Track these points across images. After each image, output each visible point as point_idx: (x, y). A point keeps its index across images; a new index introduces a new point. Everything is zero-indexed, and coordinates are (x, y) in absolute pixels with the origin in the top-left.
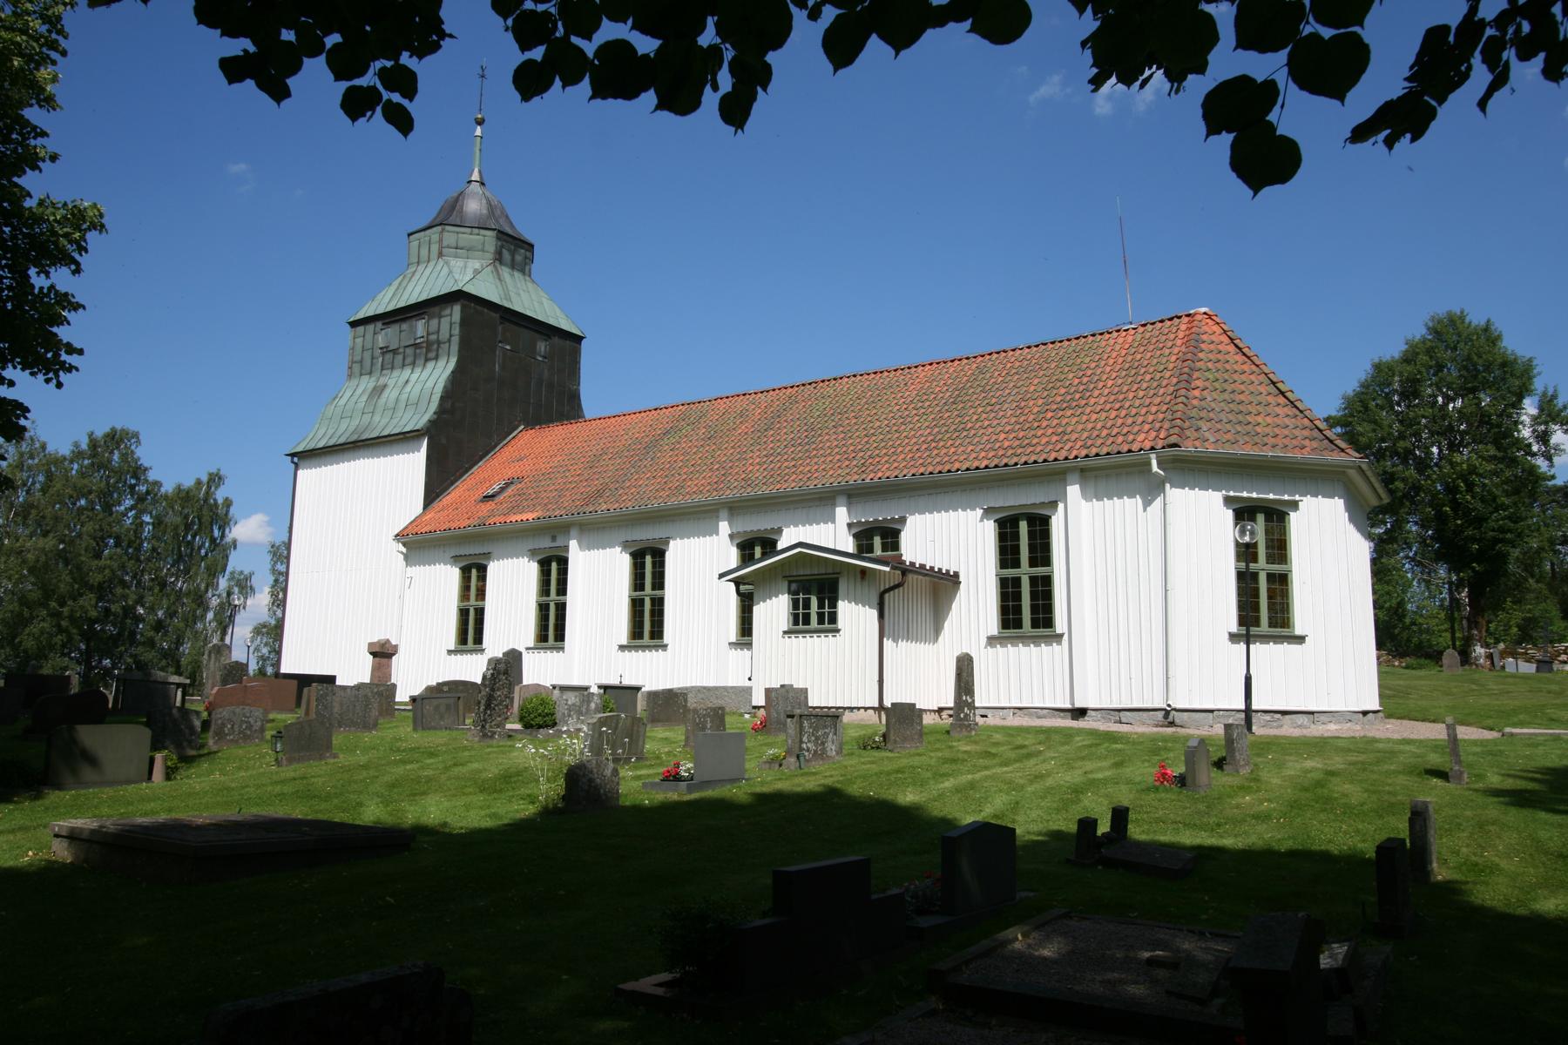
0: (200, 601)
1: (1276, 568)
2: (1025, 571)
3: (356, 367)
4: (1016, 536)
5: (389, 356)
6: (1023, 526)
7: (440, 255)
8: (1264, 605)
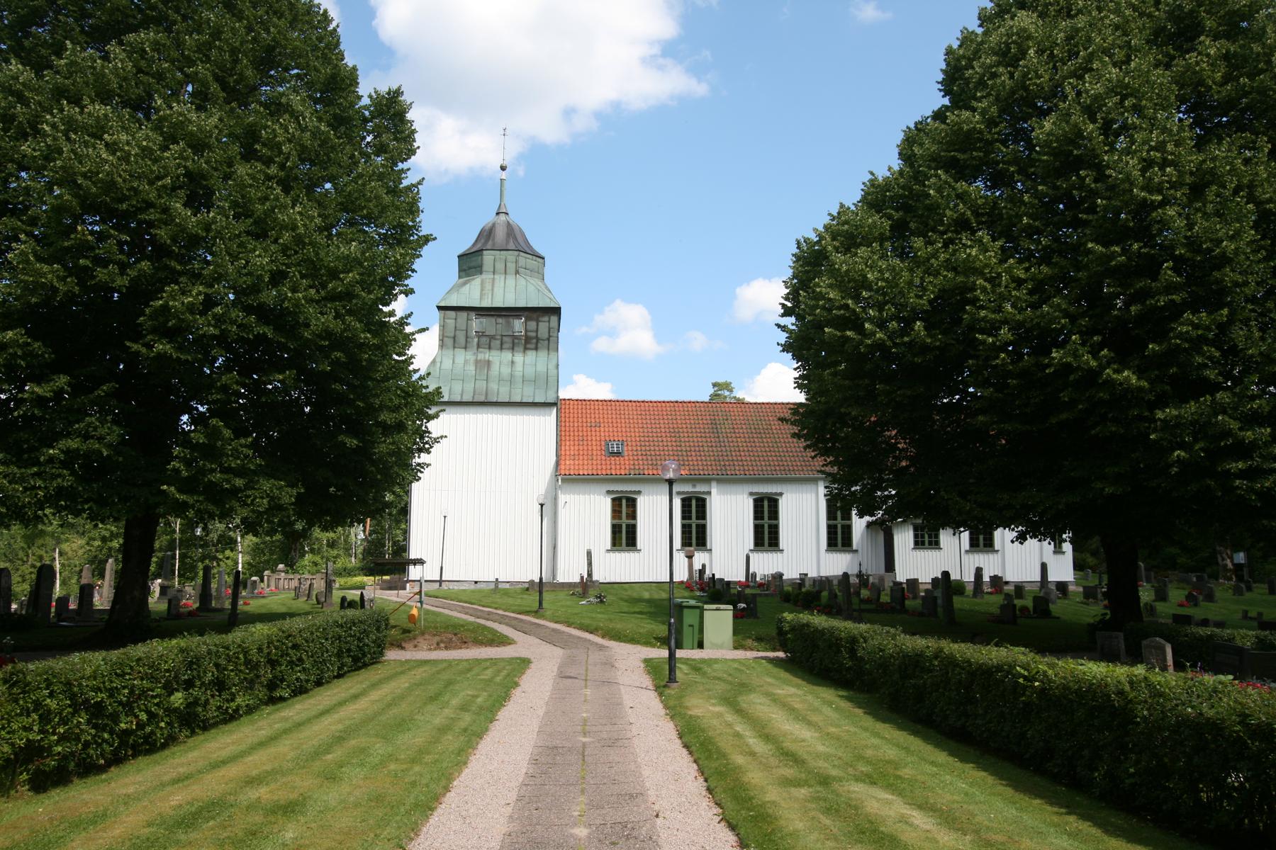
0: (77, 514)
1: (687, 522)
2: (766, 522)
3: (449, 342)
4: (762, 506)
5: (484, 340)
6: (766, 503)
7: (517, 272)
8: (624, 536)
